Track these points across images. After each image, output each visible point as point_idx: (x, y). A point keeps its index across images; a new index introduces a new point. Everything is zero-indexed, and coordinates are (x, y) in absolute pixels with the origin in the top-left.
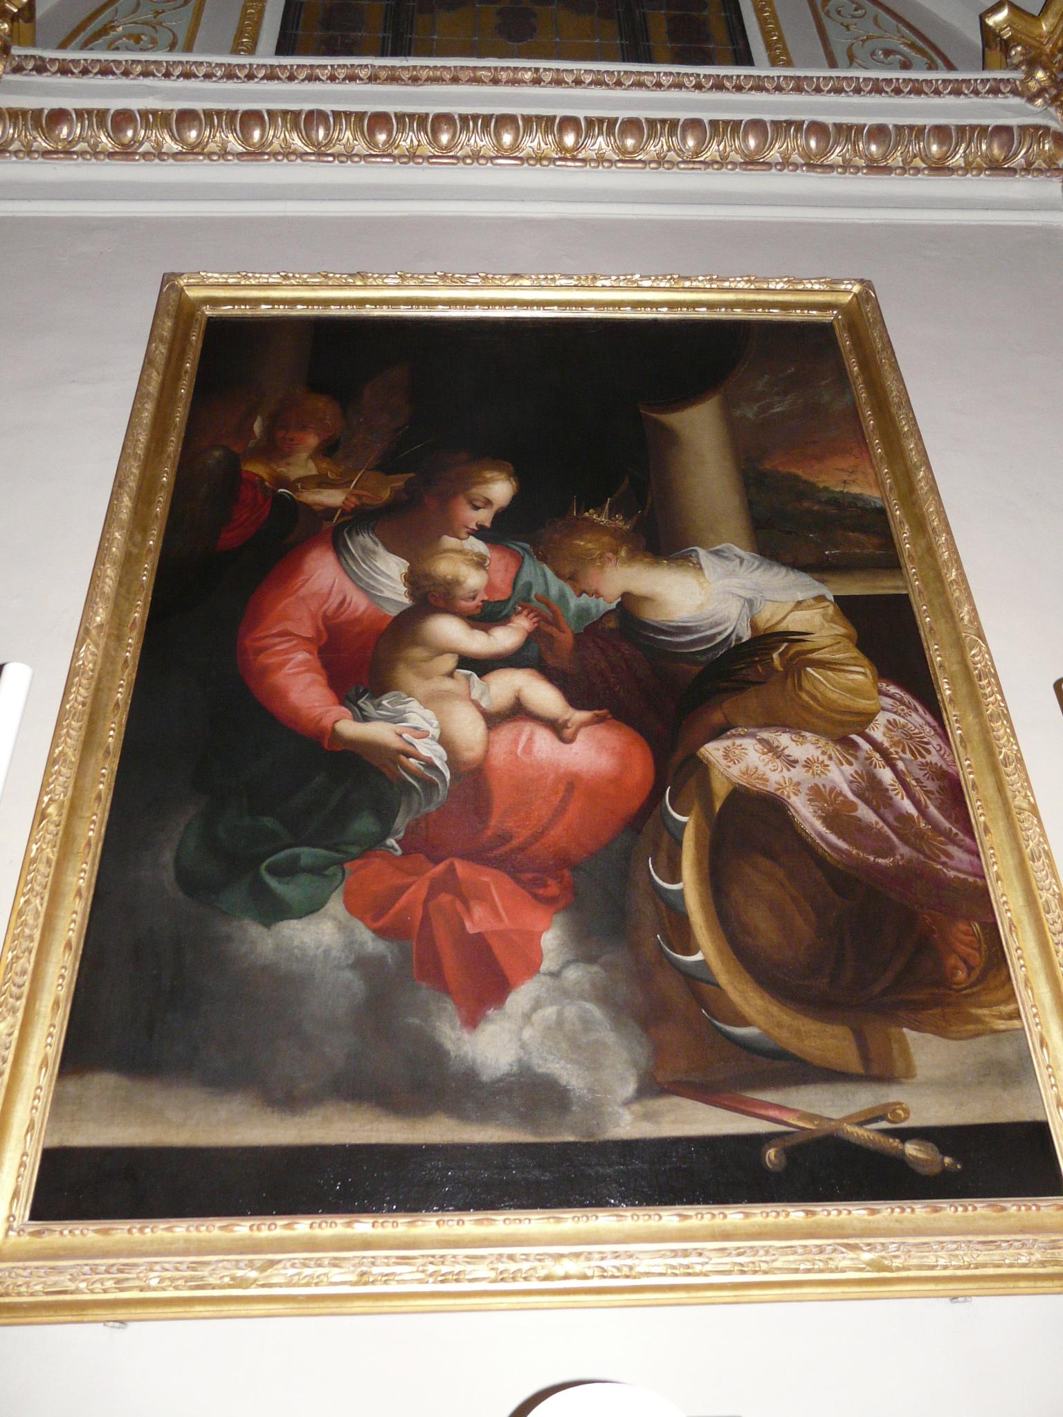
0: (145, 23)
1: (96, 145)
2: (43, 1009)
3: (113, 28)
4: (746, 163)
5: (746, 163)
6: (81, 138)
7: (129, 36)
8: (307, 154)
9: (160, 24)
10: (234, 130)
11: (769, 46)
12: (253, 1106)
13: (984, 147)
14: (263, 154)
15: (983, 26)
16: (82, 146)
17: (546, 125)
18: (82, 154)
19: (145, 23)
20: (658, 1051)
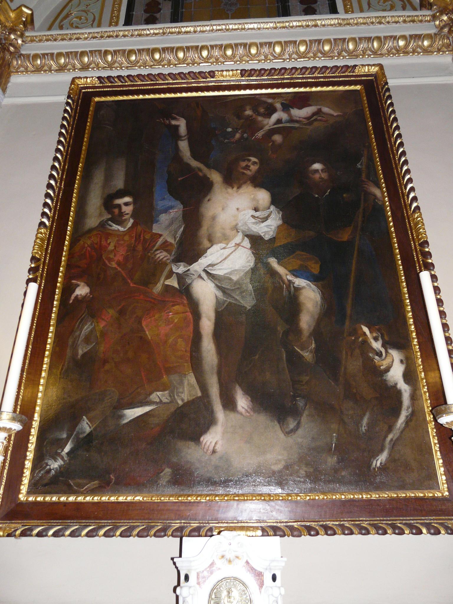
0: (82, 11)
1: (98, 64)
2: (216, 385)
3: (71, 14)
4: (82, 69)
5: (82, 69)
6: (22, 66)
7: (76, 18)
8: (106, 67)
9: (88, 11)
10: (124, 57)
11: (345, 6)
12: (259, 413)
13: (20, 62)
14: (18, 72)
15: (20, 7)
16: (22, 69)
17: (269, 46)
18: (22, 72)
19: (82, 11)
20: (397, 388)
